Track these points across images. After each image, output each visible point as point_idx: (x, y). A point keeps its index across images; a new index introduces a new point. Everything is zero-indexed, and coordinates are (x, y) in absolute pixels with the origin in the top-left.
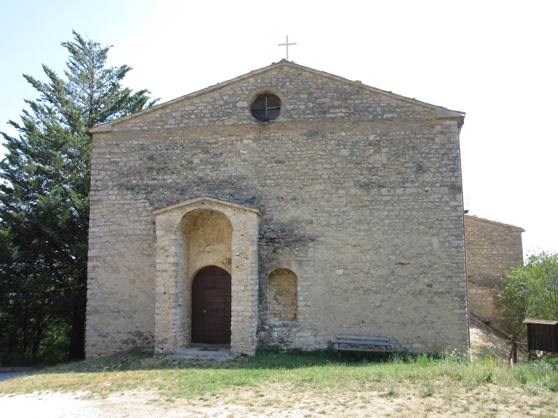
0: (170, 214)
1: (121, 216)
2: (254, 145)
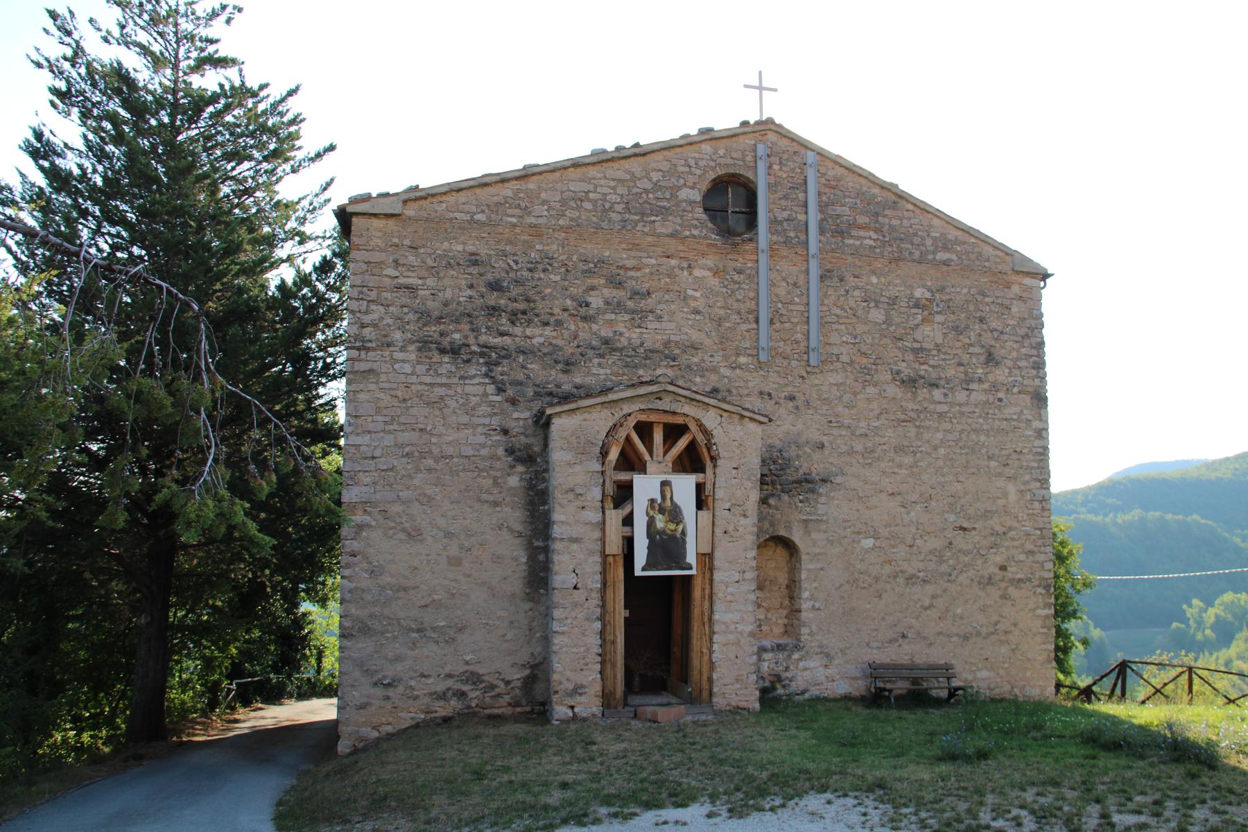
0: (586, 416)
1: (426, 411)
2: (714, 282)
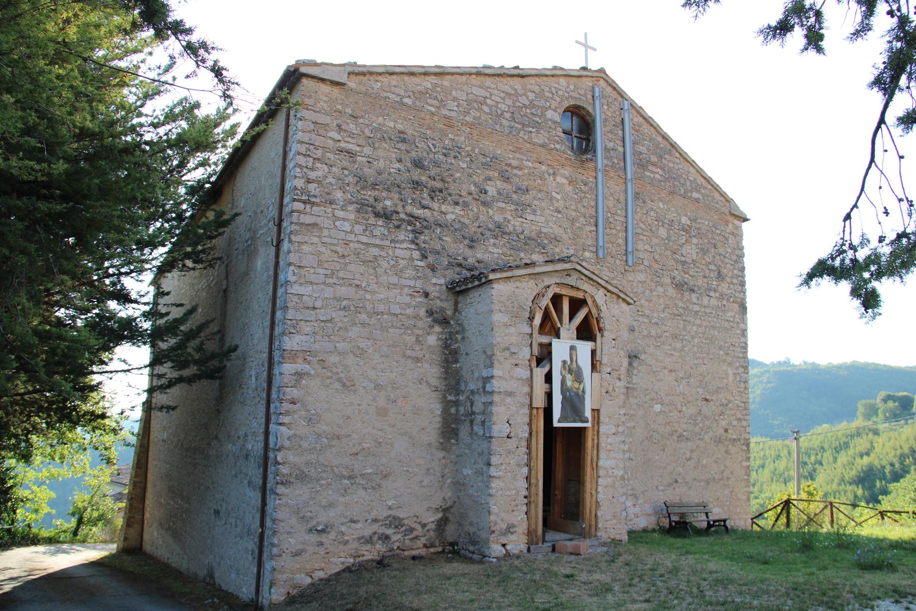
0: (518, 283)
1: (362, 269)
